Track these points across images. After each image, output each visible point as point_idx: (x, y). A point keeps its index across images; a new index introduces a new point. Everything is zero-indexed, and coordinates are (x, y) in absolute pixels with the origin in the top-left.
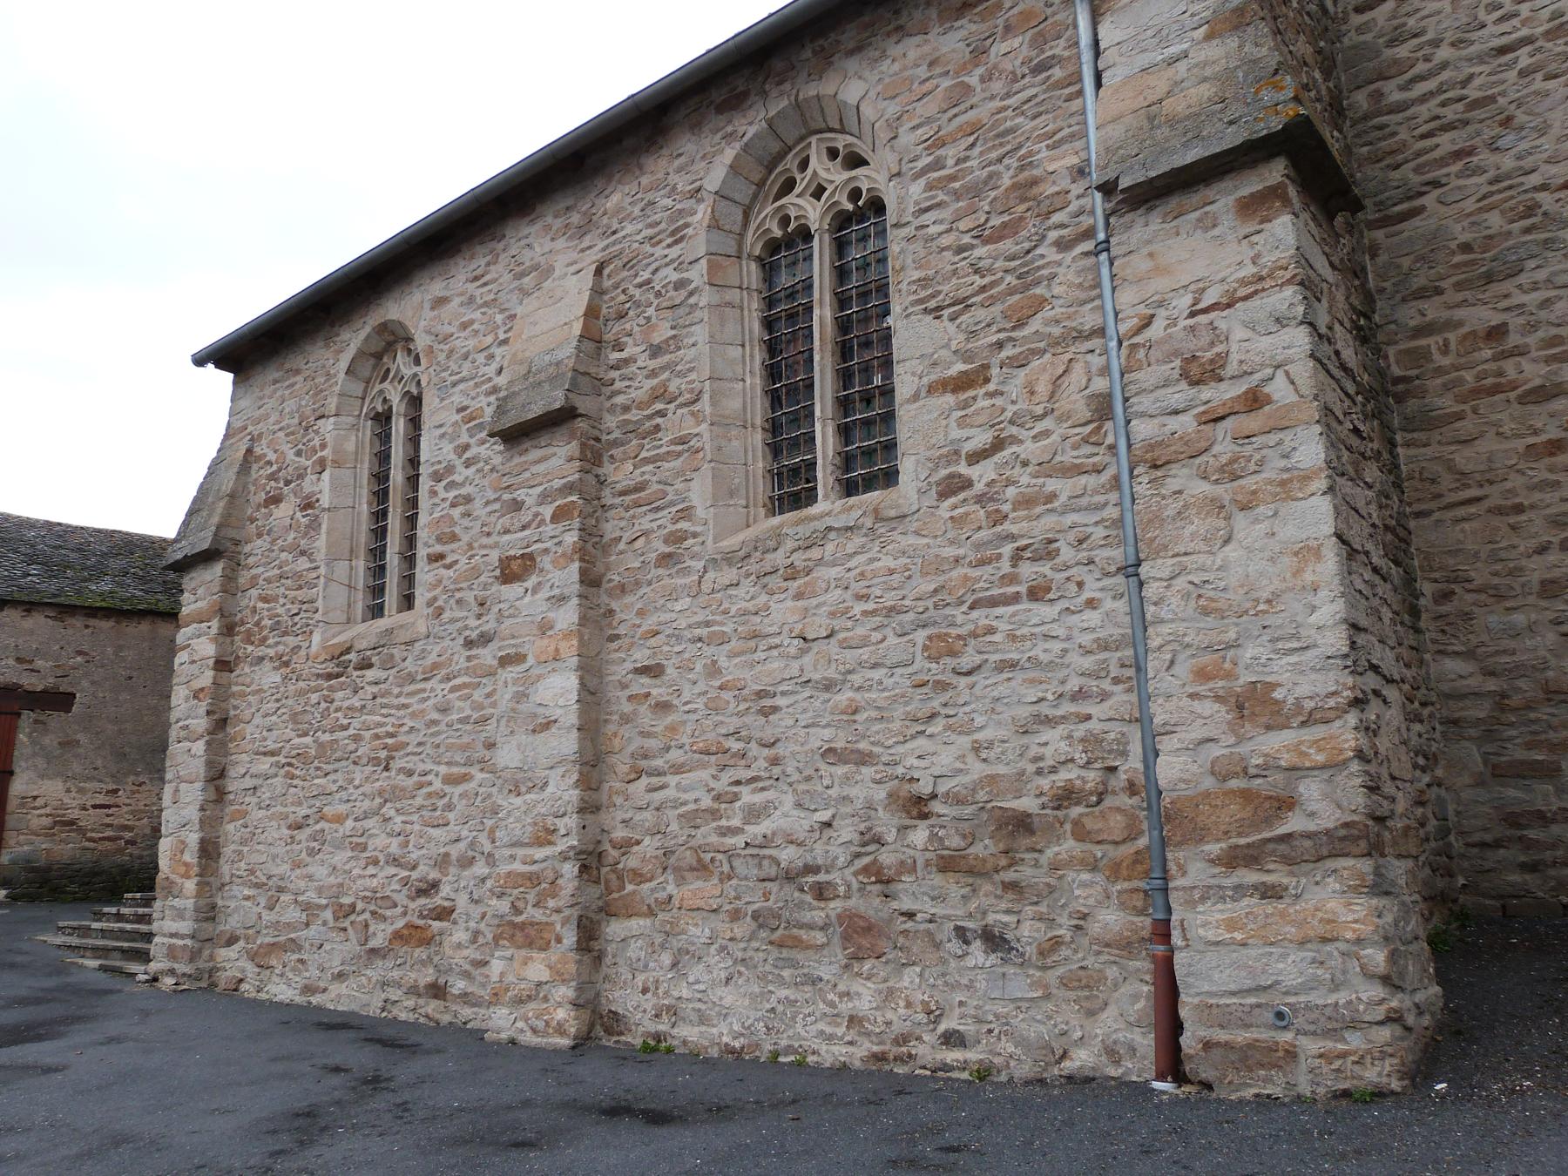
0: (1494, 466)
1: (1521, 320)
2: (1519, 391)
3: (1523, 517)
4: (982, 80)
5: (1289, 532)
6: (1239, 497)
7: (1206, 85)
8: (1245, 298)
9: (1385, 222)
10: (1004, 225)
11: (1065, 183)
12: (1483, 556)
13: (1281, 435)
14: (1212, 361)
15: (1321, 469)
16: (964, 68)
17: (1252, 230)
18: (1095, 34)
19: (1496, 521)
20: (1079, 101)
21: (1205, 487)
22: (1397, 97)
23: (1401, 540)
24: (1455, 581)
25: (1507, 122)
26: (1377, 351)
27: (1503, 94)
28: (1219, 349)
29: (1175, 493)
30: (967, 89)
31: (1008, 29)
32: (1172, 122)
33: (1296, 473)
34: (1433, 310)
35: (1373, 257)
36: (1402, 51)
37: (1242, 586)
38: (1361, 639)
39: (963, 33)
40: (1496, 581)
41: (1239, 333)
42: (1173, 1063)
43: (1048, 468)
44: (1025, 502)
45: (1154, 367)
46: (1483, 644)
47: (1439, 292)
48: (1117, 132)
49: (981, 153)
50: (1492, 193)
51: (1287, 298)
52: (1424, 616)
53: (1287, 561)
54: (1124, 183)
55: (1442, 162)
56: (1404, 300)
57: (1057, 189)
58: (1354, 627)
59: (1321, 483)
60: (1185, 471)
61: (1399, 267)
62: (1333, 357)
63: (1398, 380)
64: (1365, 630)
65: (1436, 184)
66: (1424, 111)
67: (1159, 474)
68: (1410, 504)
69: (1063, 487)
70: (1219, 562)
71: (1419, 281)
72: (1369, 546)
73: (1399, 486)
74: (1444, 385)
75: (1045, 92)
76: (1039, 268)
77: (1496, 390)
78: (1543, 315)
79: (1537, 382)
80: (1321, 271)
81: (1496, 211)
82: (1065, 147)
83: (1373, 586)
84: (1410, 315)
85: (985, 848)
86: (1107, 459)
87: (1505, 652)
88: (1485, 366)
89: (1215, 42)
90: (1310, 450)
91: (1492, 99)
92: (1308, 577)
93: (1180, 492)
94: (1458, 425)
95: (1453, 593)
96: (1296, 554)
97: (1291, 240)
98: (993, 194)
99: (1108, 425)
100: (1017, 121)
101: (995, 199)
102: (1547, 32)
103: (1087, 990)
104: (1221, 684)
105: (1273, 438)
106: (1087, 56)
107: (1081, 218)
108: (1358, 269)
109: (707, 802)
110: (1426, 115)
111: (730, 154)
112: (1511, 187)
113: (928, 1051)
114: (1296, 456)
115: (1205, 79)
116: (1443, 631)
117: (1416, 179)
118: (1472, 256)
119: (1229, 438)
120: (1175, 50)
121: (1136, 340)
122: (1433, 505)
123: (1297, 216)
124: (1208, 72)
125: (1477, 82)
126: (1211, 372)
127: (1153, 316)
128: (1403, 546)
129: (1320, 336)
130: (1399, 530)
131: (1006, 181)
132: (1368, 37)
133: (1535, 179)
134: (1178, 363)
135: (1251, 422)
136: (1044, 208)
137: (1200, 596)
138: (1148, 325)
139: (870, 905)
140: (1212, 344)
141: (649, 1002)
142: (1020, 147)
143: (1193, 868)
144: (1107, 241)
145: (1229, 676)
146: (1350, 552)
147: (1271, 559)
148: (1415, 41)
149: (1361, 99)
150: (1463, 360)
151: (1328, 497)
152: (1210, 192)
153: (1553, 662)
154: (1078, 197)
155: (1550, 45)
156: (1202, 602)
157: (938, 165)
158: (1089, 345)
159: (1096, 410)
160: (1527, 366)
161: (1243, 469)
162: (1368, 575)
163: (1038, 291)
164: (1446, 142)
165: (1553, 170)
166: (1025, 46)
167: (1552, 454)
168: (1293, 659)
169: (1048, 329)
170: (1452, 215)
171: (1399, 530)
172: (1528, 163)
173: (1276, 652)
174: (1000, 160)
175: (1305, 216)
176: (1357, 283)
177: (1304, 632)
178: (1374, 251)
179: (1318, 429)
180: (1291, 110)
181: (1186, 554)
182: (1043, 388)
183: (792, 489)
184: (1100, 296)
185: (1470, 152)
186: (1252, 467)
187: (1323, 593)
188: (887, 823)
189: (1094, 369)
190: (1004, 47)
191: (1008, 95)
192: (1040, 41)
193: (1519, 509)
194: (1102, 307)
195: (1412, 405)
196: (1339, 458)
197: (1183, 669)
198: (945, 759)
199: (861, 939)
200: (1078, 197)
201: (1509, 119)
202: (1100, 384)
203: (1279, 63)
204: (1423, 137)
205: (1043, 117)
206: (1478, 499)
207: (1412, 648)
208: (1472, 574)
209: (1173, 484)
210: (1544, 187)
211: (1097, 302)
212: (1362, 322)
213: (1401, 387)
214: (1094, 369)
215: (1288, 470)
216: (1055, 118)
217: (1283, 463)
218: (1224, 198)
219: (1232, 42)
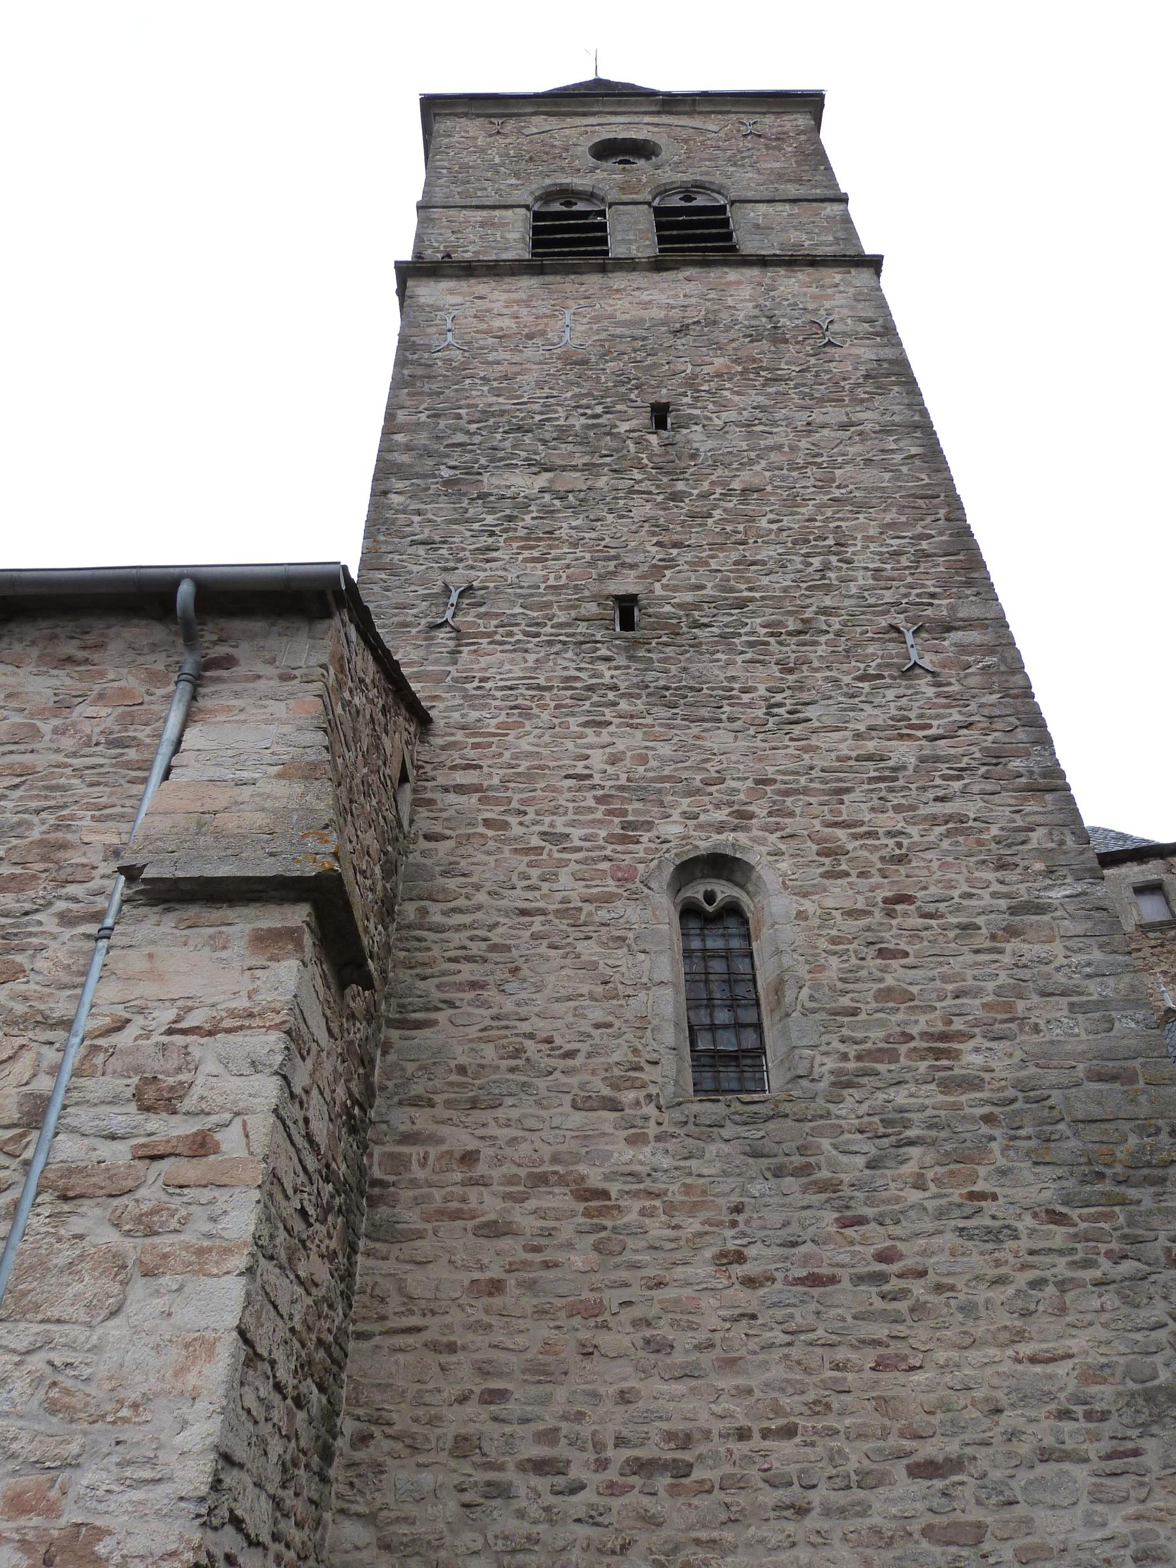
0: (439, 1295)
1: (491, 1152)
2: (477, 1221)
3: (453, 1358)
4: (55, 731)
5: (188, 1315)
6: (147, 1259)
7: (263, 815)
8: (229, 1031)
9: (403, 1024)
10: (13, 877)
11: (95, 858)
12: (409, 1395)
13: (216, 1193)
14: (172, 1088)
15: (245, 1244)
16: (42, 713)
17: (259, 963)
18: (181, 735)
19: (432, 1358)
20: (142, 787)
21: (112, 1237)
22: (437, 919)
23: (334, 1361)
24: (376, 1422)
25: (515, 971)
26: (364, 1146)
27: (517, 947)
28: (184, 1077)
29: (75, 1237)
30: (37, 733)
31: (101, 696)
32: (218, 834)
33: (218, 1242)
34: (422, 1120)
35: (385, 1053)
36: (452, 883)
37: (110, 1378)
38: (231, 1478)
39: (55, 682)
40: (415, 1428)
41: (210, 1066)
45: (107, 1078)
46: (386, 1507)
47: (431, 1104)
48: (162, 824)
49: (21, 798)
50: (492, 1028)
51: (268, 1043)
52: (336, 1460)
53: (174, 1354)
54: (148, 873)
55: (459, 987)
56: (400, 1103)
57: (84, 860)
58: (227, 1459)
59: (240, 1261)
60: (98, 1211)
61: (403, 1069)
62: (301, 1123)
63: (376, 1183)
64: (241, 1466)
65: (451, 1004)
66: (457, 938)
67: (66, 1208)
68: (354, 1322)
70: (94, 1340)
71: (417, 1089)
72: (279, 1355)
73: (348, 1298)
74: (415, 1198)
75: (113, 766)
76: (31, 934)
77: (456, 1215)
78: (509, 1151)
79: (492, 1216)
80: (314, 1030)
81: (492, 1045)
82: (109, 824)
83: (269, 1408)
84: (401, 1119)
86: (16, 1177)
87: (405, 1519)
88: (453, 1189)
89: (284, 782)
90: (240, 1217)
91: (508, 948)
92: (191, 1379)
93: (81, 1237)
94: (418, 1243)
95: (372, 1436)
96: (187, 1346)
97: (291, 985)
98: (15, 842)
99: (34, 1135)
100: (72, 781)
101: (15, 847)
102: (557, 911)
104: (36, 1521)
105: (206, 1195)
106: (166, 749)
107: (97, 898)
108: (366, 1059)
110: (456, 943)
112: (507, 1027)
114: (224, 1222)
115: (263, 810)
116: (351, 1484)
117: (436, 995)
118: (464, 1079)
119: (160, 1182)
120: (246, 775)
121: (100, 1042)
122: (376, 1327)
123: (305, 965)
124: (268, 804)
125: (500, 930)
127: (128, 1021)
128: (335, 1369)
129: (293, 1096)
130: (336, 1351)
131: (35, 834)
132: (428, 862)
133: (525, 1027)
134: (135, 1080)
135: (188, 1170)
136: (63, 875)
137: (54, 1384)
138: (119, 1029)
140: (179, 1070)
142: (64, 806)
144: (112, 929)
145: (51, 1510)
146: (251, 1355)
147: (157, 1348)
148: (463, 879)
149: (410, 910)
150: (436, 1178)
151: (243, 1280)
152: (230, 913)
153: (448, 1539)
154: (103, 877)
155: (557, 921)
156: (54, 1393)
158: (49, 1035)
159: (28, 1113)
160: (487, 1198)
161: (162, 1224)
162: (266, 1390)
163: (19, 958)
164: (468, 972)
165: (541, 1024)
166: (111, 718)
167: (490, 1294)
168: (138, 1495)
169: (12, 1004)
170: (455, 1036)
171: (336, 1351)
172: (523, 1011)
173: (120, 1481)
174: (38, 812)
175: (315, 970)
176: (361, 1071)
177: (163, 1457)
178: (386, 1049)
179: (256, 1195)
180: (329, 863)
181: (59, 1321)
184: (83, 986)
185: (482, 986)
186: (173, 1224)
187: (201, 1405)
189: (45, 1065)
190: (91, 711)
191: (74, 755)
192: (127, 720)
193: (452, 1348)
194: (79, 998)
195: (383, 1212)
196: (272, 1237)
200: (103, 877)
201: (517, 969)
202: (44, 1084)
203: (332, 820)
204: (451, 960)
205: (101, 788)
206: (419, 1330)
207: (311, 1501)
208: (394, 1416)
209: (76, 1225)
210: (531, 1036)
211: (78, 991)
212: (356, 1111)
213: (377, 1191)
214: (45, 1065)
215: (210, 1236)
216: (112, 794)
217: (208, 1227)
218: (245, 922)
219: (299, 788)
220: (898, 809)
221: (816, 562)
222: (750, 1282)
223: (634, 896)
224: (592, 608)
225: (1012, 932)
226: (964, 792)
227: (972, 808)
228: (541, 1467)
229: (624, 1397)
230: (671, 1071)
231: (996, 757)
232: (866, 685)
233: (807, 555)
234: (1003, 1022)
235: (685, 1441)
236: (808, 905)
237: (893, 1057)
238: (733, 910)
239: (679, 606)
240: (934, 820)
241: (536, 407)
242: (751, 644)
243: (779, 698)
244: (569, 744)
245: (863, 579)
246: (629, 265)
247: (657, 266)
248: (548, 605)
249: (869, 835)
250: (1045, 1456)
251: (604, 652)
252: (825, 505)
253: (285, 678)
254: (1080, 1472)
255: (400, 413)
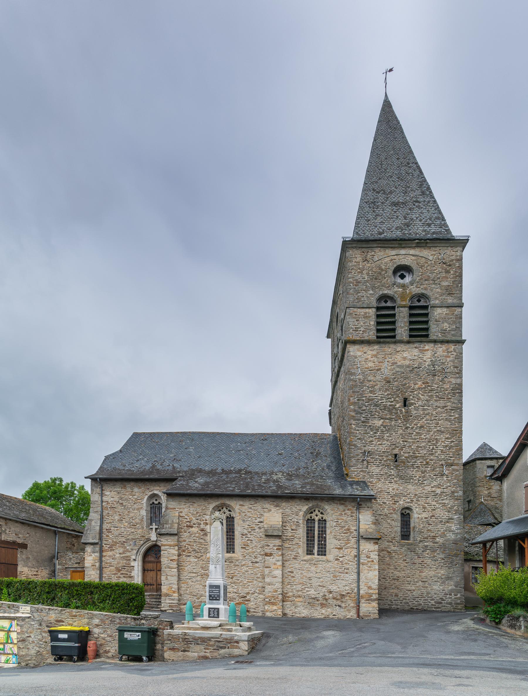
5: (374, 574)
30: (342, 515)
42: (358, 616)
43: (349, 561)
44: (346, 563)
69: (351, 563)
85: (339, 597)
103: (349, 611)
109: (300, 589)
111: (307, 507)
113: (331, 616)
126: (369, 557)
135: (372, 563)
139: (324, 602)
141: (291, 612)
143: (363, 601)
157: (338, 522)
182: (349, 552)
183: (310, 552)
188: (327, 594)
197: (364, 584)
198: (334, 588)
199: (322, 605)
218: (372, 542)
220: (436, 501)
221: (431, 447)
222: (406, 563)
223: (395, 513)
224: (390, 457)
225: (448, 522)
226: (446, 499)
227: (446, 502)
228: (383, 578)
229: (392, 573)
230: (398, 538)
231: (453, 492)
232: (435, 477)
233: (430, 445)
234: (443, 535)
235: (398, 577)
236: (420, 516)
237: (427, 538)
238: (408, 514)
239: (405, 457)
240: (440, 503)
241: (379, 398)
242: (417, 467)
243: (420, 479)
244: (386, 486)
245: (439, 452)
246: (401, 342)
247: (408, 342)
248: (382, 456)
249: (431, 505)
250: (435, 581)
251: (392, 467)
252: (435, 432)
253: (368, 507)
254: (439, 583)
255: (351, 398)
